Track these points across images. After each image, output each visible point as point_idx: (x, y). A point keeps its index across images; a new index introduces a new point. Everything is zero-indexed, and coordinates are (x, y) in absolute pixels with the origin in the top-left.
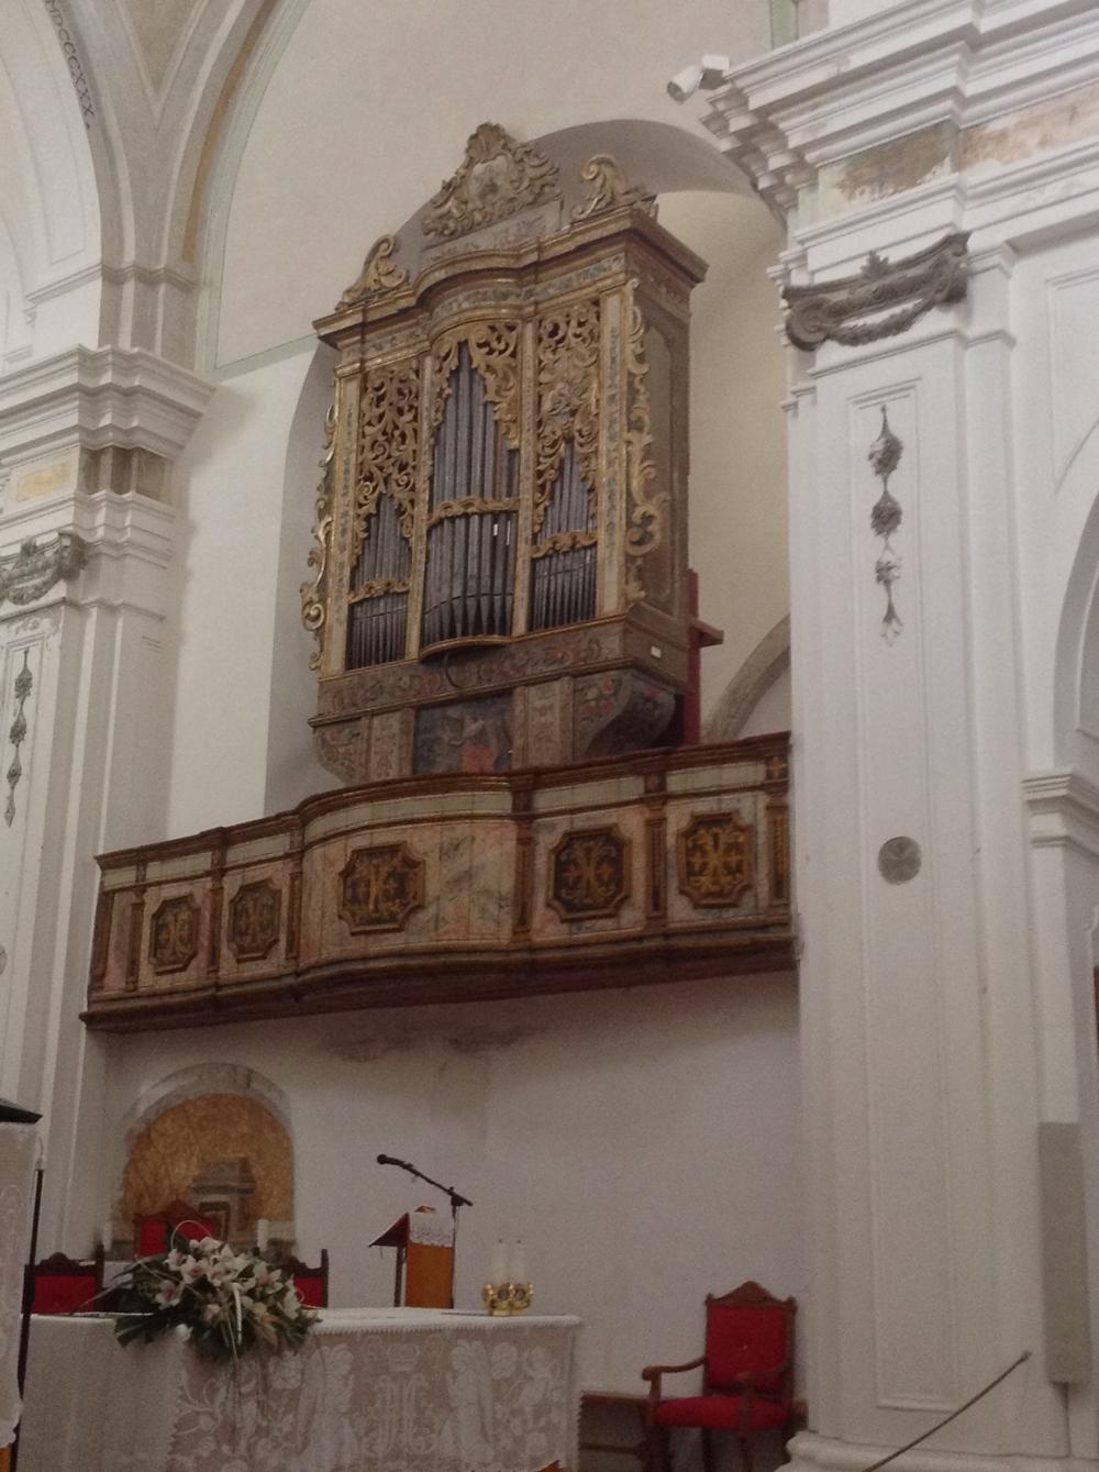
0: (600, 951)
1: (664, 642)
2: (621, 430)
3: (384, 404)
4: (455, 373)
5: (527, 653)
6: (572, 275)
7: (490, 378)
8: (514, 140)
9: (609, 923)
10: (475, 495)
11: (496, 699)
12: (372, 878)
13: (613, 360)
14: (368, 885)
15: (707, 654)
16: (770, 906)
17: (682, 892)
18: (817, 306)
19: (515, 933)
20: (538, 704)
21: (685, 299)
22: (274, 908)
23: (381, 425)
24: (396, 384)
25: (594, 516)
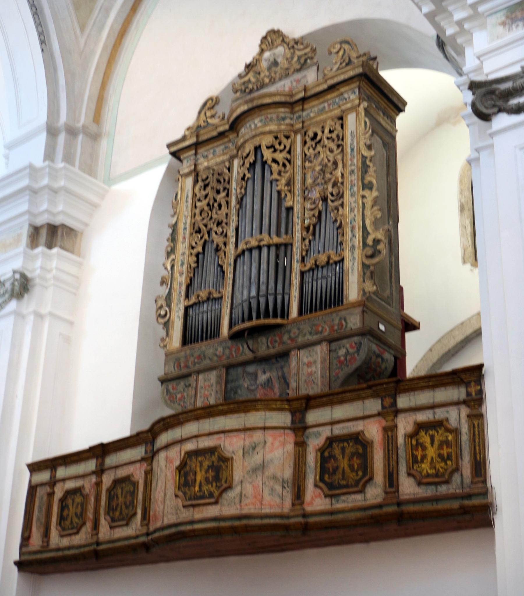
0: (352, 516)
1: (386, 322)
2: (358, 191)
3: (209, 189)
4: (253, 165)
5: (299, 329)
6: (326, 105)
7: (274, 166)
8: (288, 37)
9: (359, 497)
10: (265, 236)
11: (278, 359)
12: (198, 469)
13: (352, 150)
14: (195, 474)
15: (409, 336)
16: (472, 482)
17: (409, 474)
18: (492, 92)
19: (293, 505)
20: (306, 360)
21: (394, 122)
22: (133, 494)
23: (207, 201)
24: (216, 176)
25: (341, 243)
